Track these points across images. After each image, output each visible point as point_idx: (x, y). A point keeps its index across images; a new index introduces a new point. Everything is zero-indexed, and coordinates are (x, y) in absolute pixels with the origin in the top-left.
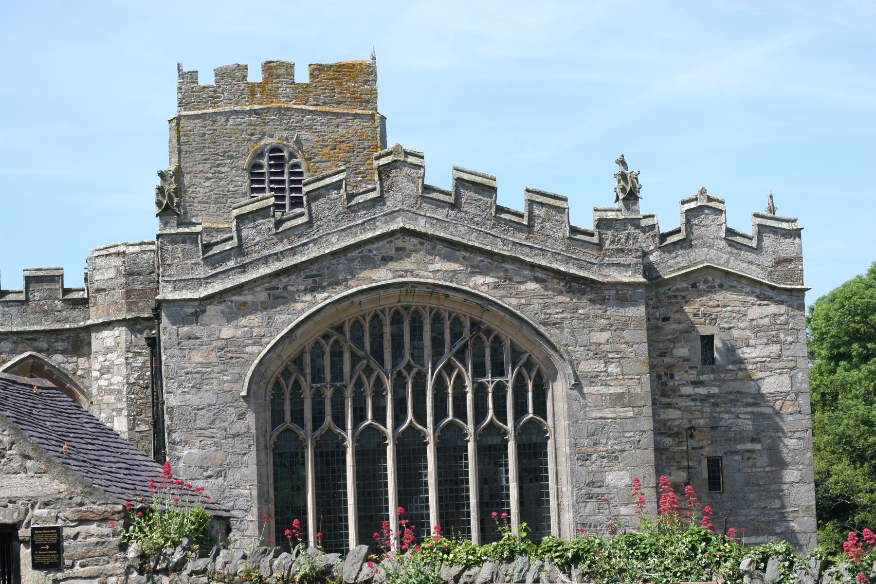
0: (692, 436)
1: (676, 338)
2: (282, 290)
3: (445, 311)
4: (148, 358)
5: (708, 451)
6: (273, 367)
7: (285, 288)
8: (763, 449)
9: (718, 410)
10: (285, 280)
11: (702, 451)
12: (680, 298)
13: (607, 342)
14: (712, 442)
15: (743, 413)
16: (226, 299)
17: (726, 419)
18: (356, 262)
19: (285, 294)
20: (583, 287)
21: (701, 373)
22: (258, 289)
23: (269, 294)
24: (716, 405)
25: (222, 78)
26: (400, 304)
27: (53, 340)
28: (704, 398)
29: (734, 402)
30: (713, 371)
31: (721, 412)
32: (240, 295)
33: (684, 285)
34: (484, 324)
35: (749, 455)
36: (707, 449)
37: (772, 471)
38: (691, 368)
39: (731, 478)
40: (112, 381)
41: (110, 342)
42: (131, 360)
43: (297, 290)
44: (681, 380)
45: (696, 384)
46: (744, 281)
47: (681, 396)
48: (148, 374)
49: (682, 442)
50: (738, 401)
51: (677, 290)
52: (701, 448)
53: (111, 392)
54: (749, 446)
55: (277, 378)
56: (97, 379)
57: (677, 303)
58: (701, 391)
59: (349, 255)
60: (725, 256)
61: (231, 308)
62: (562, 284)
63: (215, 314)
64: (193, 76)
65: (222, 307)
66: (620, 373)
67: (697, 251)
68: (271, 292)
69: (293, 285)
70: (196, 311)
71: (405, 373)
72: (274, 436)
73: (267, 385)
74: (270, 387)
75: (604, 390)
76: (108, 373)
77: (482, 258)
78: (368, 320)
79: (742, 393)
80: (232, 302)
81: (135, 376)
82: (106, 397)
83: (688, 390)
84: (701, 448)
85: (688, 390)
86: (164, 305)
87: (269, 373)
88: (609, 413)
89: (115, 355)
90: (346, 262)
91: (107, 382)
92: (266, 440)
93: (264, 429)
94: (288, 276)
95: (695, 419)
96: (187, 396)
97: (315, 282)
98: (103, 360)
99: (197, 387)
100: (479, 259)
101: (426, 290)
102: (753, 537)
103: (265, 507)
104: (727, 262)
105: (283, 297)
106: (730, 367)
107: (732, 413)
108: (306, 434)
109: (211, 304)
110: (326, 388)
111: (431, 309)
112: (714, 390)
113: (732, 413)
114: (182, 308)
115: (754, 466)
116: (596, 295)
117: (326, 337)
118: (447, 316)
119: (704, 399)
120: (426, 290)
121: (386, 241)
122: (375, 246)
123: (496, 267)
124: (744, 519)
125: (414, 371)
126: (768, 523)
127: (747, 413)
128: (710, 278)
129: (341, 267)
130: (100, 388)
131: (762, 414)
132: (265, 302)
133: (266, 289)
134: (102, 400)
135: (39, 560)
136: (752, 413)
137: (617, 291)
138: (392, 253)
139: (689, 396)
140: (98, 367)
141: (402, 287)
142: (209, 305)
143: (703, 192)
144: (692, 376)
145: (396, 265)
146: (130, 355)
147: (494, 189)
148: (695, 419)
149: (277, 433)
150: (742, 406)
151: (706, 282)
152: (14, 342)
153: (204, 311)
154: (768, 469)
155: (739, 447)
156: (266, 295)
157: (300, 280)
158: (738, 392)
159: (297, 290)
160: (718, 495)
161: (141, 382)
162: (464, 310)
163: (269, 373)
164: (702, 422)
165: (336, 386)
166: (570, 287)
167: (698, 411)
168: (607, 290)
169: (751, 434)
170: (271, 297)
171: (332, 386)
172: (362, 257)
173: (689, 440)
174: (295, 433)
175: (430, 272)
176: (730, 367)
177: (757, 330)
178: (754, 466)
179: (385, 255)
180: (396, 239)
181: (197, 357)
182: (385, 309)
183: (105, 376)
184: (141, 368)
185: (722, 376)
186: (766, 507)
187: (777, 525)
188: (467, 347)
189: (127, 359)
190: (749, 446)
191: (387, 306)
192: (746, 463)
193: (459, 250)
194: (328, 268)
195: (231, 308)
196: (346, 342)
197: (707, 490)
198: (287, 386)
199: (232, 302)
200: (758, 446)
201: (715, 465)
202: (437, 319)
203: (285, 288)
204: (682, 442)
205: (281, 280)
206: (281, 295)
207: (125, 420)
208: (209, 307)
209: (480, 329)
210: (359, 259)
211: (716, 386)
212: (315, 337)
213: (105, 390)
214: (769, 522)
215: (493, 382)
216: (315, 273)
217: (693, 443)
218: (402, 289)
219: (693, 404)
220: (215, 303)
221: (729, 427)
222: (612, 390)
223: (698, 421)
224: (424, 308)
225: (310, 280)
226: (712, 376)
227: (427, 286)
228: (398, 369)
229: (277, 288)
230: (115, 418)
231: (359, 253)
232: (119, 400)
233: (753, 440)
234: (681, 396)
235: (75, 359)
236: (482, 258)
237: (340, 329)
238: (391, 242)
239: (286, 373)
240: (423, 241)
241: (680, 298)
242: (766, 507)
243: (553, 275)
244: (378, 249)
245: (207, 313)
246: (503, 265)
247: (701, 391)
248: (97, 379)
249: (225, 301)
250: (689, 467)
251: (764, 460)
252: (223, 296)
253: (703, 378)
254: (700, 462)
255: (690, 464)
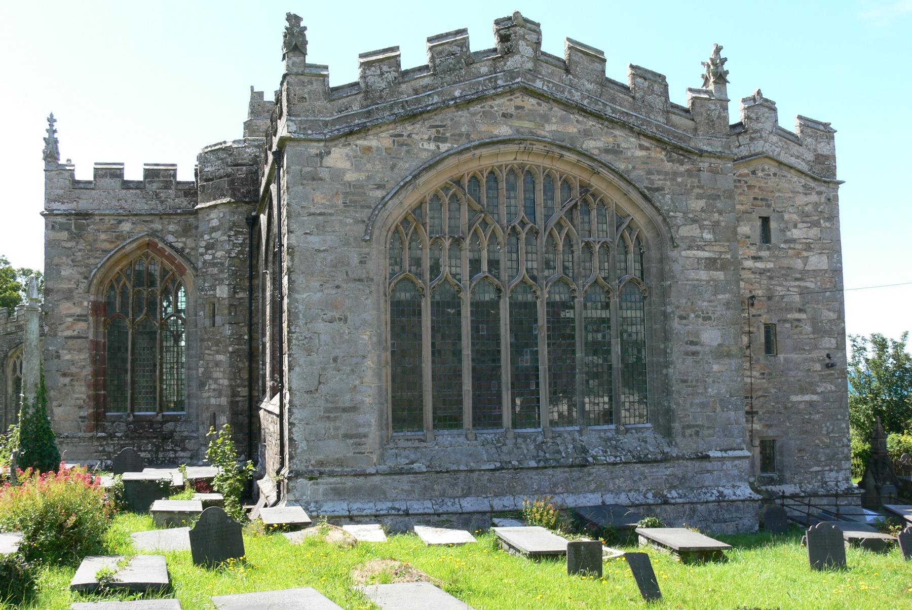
0: (753, 305)
1: (740, 217)
2: (406, 138)
3: (557, 171)
4: (247, 236)
5: (764, 318)
6: (394, 216)
7: (409, 136)
8: (808, 319)
9: (773, 282)
10: (409, 128)
11: (760, 318)
12: (743, 182)
13: (702, 210)
14: (768, 311)
15: (792, 287)
16: (351, 143)
17: (780, 290)
18: (478, 117)
19: (409, 142)
20: (682, 157)
21: (760, 249)
22: (383, 135)
23: (394, 141)
24: (771, 278)
25: (104, 176)
26: (515, 162)
27: (166, 223)
28: (762, 271)
29: (785, 276)
30: (769, 249)
31: (776, 285)
32: (365, 139)
33: (746, 171)
34: (592, 186)
35: (796, 323)
36: (764, 317)
37: (814, 339)
38: (752, 244)
39: (782, 341)
40: (216, 255)
41: (215, 223)
42: (233, 238)
43: (421, 139)
44: (743, 254)
45: (756, 258)
46: (792, 171)
47: (743, 269)
48: (247, 249)
49: (744, 309)
50: (788, 276)
51: (740, 175)
52: (760, 315)
53: (214, 265)
54: (797, 315)
55: (397, 227)
56: (202, 255)
57: (741, 186)
58: (760, 265)
59: (472, 109)
60: (778, 150)
61: (356, 151)
62: (664, 153)
63: (339, 156)
64: (261, 94)
65: (346, 150)
66: (713, 240)
67: (756, 142)
68: (396, 139)
69: (417, 134)
70: (321, 153)
71: (519, 228)
72: (393, 284)
73: (388, 232)
74: (390, 234)
75: (701, 254)
76: (212, 248)
77: (594, 123)
78: (485, 174)
79: (791, 269)
80: (356, 146)
81: (236, 251)
82: (210, 269)
83: (749, 264)
84: (760, 315)
85: (749, 264)
86: (288, 143)
87: (391, 220)
88: (703, 275)
89: (219, 233)
90: (468, 115)
91: (211, 256)
92: (385, 287)
93: (384, 276)
94: (413, 124)
95: (754, 290)
96: (311, 238)
97: (438, 132)
98: (208, 238)
99: (321, 229)
100: (591, 123)
101: (543, 148)
102: (800, 396)
103: (383, 355)
104: (779, 154)
105: (407, 145)
106: (782, 245)
107: (784, 286)
108: (424, 282)
109: (335, 146)
110: (445, 238)
111: (545, 169)
112: (770, 265)
113: (784, 286)
114: (306, 149)
115: (801, 333)
116: (692, 166)
117: (446, 188)
118: (558, 177)
119: (762, 272)
120: (543, 148)
121: (506, 99)
122: (497, 102)
123: (606, 133)
124: (792, 379)
125: (528, 227)
126: (811, 384)
127: (795, 287)
128: (766, 167)
129: (463, 119)
130: (205, 262)
131: (807, 288)
132: (390, 148)
133: (391, 136)
134: (206, 272)
135: (597, 66)
136: (799, 286)
137: (711, 164)
138: (512, 110)
139: (750, 269)
140: (203, 244)
141: (521, 143)
142: (334, 147)
143: (759, 92)
144: (753, 251)
145: (517, 123)
146: (232, 233)
147: (605, 61)
148: (754, 290)
149: (395, 281)
150: (792, 281)
151: (763, 170)
152: (133, 223)
153: (329, 153)
154: (811, 336)
155: (789, 316)
156: (391, 142)
157: (424, 129)
158: (788, 268)
159: (421, 139)
160: (773, 358)
161: (241, 256)
162: (575, 172)
163: (391, 220)
164: (760, 293)
165: (454, 237)
166: (670, 157)
167: (757, 283)
168: (702, 162)
169: (799, 306)
170: (396, 144)
171: (451, 237)
172: (484, 112)
173: (750, 308)
174: (412, 282)
175: (548, 132)
176: (782, 245)
177: (804, 215)
178: (801, 333)
179: (505, 112)
180: (516, 98)
181: (319, 198)
182: (502, 165)
183: (210, 252)
184: (241, 245)
185: (776, 253)
186: (810, 370)
187: (818, 386)
188: (576, 208)
189: (229, 236)
190: (797, 315)
191: (504, 163)
192: (796, 331)
193: (573, 113)
194: (452, 120)
195: (356, 151)
196: (465, 195)
197: (764, 353)
198: (407, 235)
199: (356, 146)
200: (803, 316)
201: (769, 330)
202: (549, 176)
203: (409, 136)
204: (744, 309)
205: (406, 128)
206: (405, 143)
207: (227, 288)
208: (333, 149)
209: (588, 191)
210: (481, 114)
211: (770, 261)
212: (435, 188)
213: (209, 263)
214: (812, 383)
215: (599, 242)
216: (439, 123)
217: (753, 311)
218: (521, 146)
219: (752, 276)
220: (340, 146)
221: (783, 297)
222: (706, 254)
223: (757, 292)
224: (538, 167)
225: (434, 130)
226: (768, 253)
227: (544, 144)
228: (513, 225)
229: (401, 136)
230: (218, 287)
231: (481, 108)
232: (222, 272)
233: (800, 310)
234: (743, 269)
235: (184, 239)
236: (594, 123)
237: (458, 182)
238: (511, 100)
239: (405, 221)
240: (540, 101)
241: (743, 182)
242: (810, 370)
243: (656, 144)
244: (499, 105)
245: (332, 155)
246: (612, 131)
247: (760, 265)
248: (202, 255)
249: (350, 144)
250: (750, 332)
251: (808, 328)
252: (348, 139)
253: (763, 254)
254: (758, 328)
255: (751, 329)
